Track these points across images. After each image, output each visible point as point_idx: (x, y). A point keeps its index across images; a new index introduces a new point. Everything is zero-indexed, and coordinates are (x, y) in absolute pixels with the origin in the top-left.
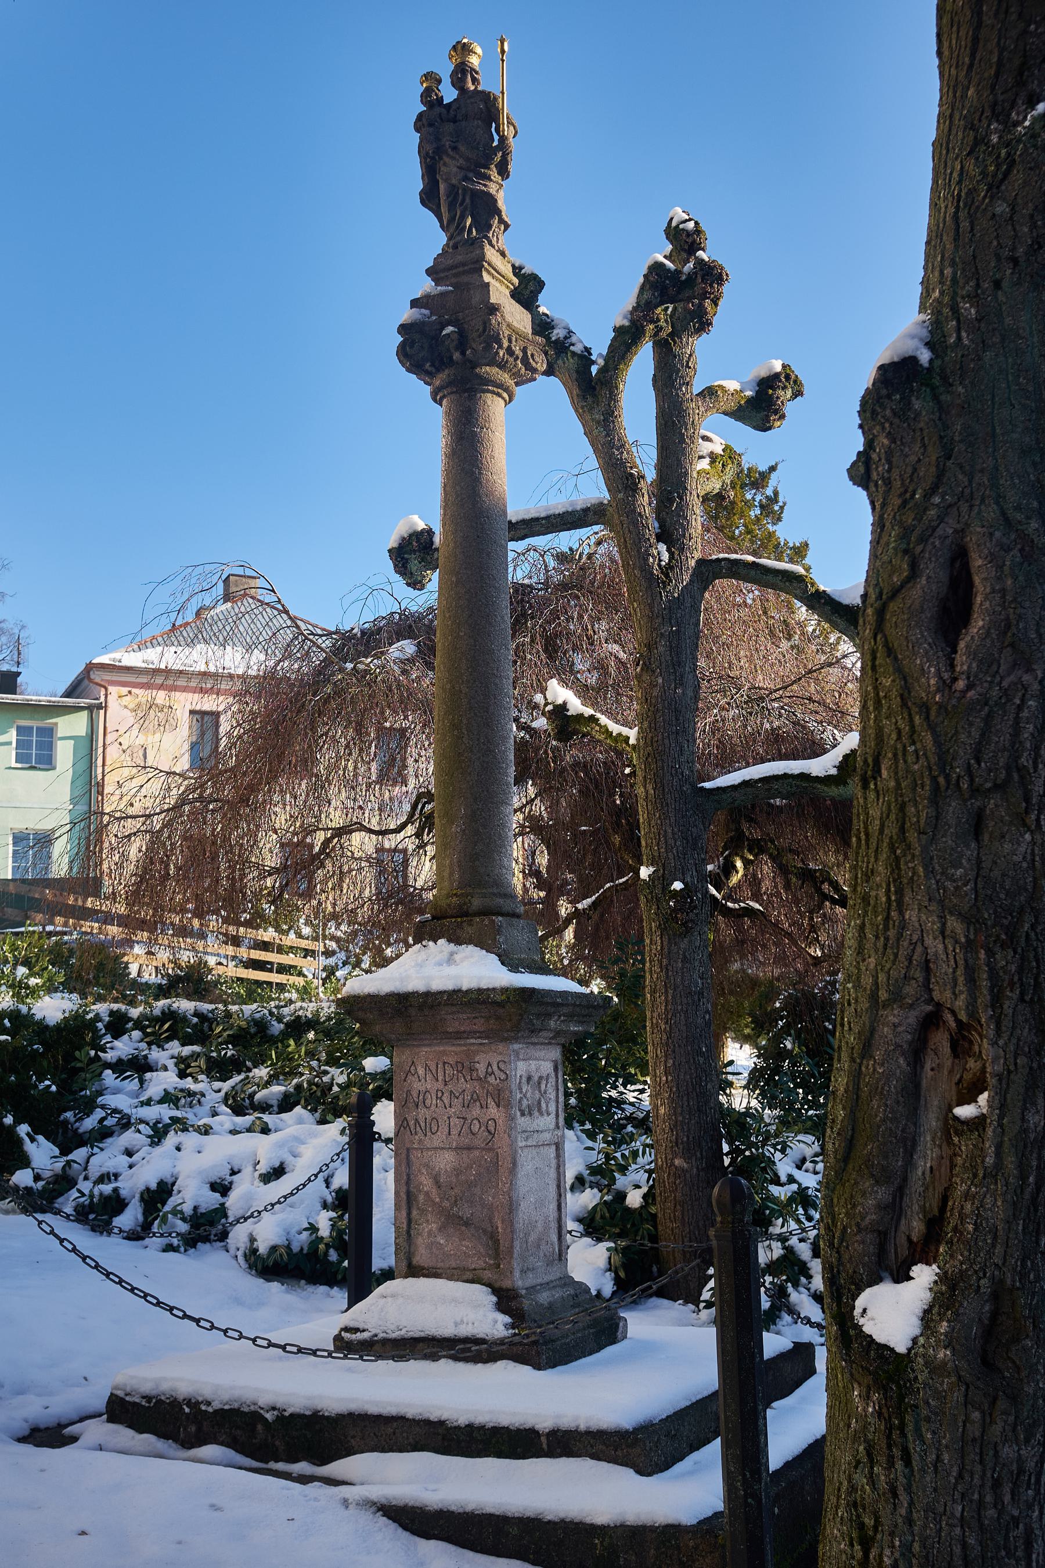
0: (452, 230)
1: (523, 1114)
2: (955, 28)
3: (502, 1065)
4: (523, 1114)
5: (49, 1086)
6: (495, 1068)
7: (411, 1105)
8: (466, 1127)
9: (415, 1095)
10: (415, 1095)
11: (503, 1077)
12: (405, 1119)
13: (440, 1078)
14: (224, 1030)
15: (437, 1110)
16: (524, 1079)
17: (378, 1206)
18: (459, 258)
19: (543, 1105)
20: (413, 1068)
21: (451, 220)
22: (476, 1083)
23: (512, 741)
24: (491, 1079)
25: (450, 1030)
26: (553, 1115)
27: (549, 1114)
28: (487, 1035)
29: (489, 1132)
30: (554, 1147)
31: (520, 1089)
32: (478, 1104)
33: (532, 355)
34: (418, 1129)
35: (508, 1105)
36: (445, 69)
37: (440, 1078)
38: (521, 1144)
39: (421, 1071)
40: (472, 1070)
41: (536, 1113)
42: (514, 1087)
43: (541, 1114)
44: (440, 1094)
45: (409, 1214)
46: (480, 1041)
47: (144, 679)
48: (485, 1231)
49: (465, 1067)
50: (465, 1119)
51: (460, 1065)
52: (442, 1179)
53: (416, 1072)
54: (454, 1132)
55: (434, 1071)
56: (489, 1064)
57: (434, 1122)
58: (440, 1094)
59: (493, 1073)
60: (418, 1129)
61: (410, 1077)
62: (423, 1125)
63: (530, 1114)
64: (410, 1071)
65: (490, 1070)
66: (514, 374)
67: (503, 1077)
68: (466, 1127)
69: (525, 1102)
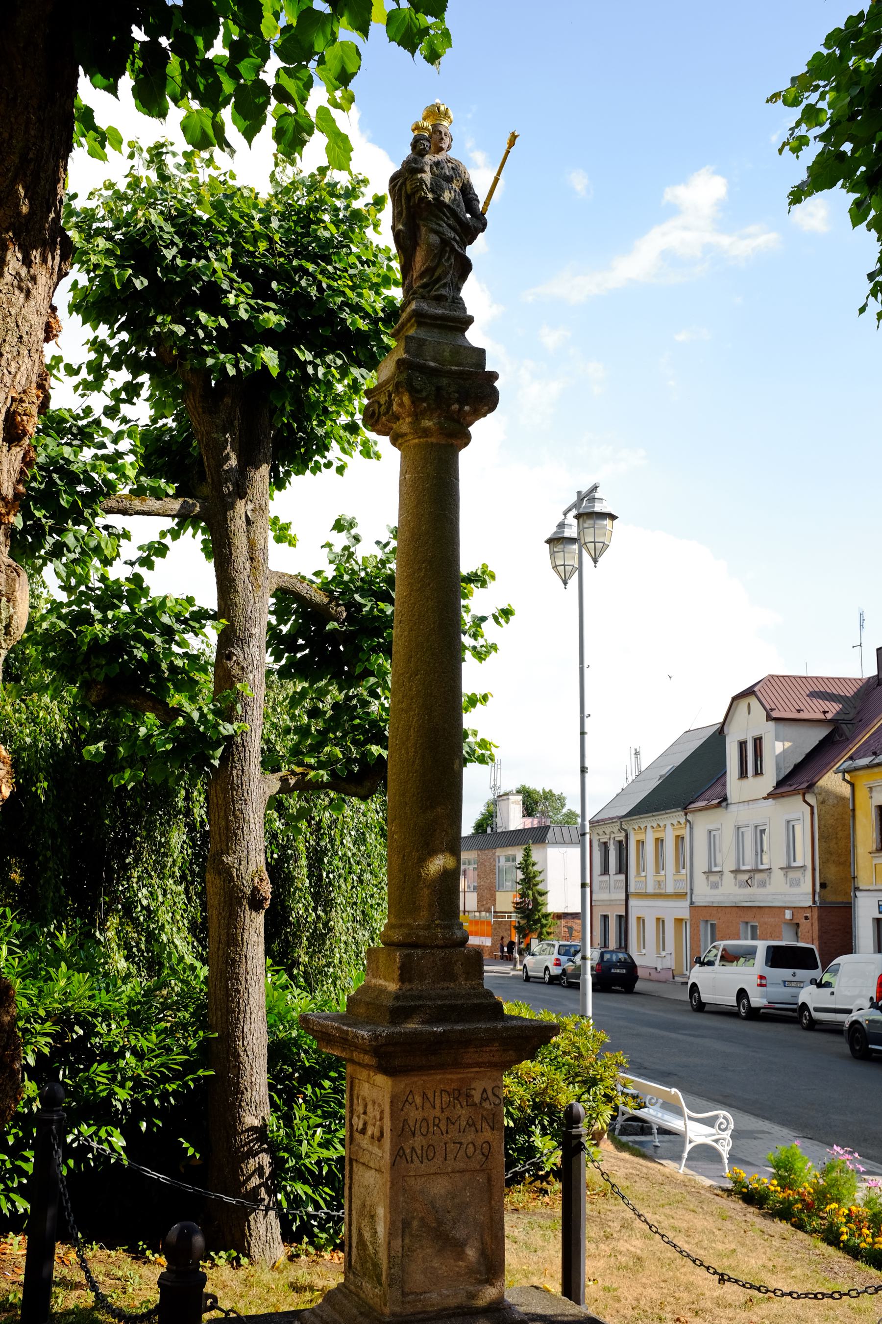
5: (69, 1103)
6: (489, 1092)
8: (461, 1153)
10: (411, 1123)
12: (402, 1147)
13: (438, 1105)
14: (305, 899)
15: (434, 1137)
20: (410, 1097)
23: (390, 784)
24: (486, 1105)
25: (153, 176)
29: (483, 1154)
32: (473, 1129)
34: (414, 1157)
37: (438, 1105)
39: (418, 1100)
40: (469, 1096)
44: (437, 1121)
47: (614, 903)
49: (461, 1094)
50: (461, 1144)
51: (456, 1092)
53: (414, 1101)
54: (450, 1156)
55: (431, 1100)
56: (485, 1090)
57: (424, 1124)
58: (437, 1121)
59: (487, 1098)
60: (414, 1157)
61: (407, 1106)
62: (419, 1152)
64: (407, 1100)
66: (271, 1032)
68: (461, 1153)
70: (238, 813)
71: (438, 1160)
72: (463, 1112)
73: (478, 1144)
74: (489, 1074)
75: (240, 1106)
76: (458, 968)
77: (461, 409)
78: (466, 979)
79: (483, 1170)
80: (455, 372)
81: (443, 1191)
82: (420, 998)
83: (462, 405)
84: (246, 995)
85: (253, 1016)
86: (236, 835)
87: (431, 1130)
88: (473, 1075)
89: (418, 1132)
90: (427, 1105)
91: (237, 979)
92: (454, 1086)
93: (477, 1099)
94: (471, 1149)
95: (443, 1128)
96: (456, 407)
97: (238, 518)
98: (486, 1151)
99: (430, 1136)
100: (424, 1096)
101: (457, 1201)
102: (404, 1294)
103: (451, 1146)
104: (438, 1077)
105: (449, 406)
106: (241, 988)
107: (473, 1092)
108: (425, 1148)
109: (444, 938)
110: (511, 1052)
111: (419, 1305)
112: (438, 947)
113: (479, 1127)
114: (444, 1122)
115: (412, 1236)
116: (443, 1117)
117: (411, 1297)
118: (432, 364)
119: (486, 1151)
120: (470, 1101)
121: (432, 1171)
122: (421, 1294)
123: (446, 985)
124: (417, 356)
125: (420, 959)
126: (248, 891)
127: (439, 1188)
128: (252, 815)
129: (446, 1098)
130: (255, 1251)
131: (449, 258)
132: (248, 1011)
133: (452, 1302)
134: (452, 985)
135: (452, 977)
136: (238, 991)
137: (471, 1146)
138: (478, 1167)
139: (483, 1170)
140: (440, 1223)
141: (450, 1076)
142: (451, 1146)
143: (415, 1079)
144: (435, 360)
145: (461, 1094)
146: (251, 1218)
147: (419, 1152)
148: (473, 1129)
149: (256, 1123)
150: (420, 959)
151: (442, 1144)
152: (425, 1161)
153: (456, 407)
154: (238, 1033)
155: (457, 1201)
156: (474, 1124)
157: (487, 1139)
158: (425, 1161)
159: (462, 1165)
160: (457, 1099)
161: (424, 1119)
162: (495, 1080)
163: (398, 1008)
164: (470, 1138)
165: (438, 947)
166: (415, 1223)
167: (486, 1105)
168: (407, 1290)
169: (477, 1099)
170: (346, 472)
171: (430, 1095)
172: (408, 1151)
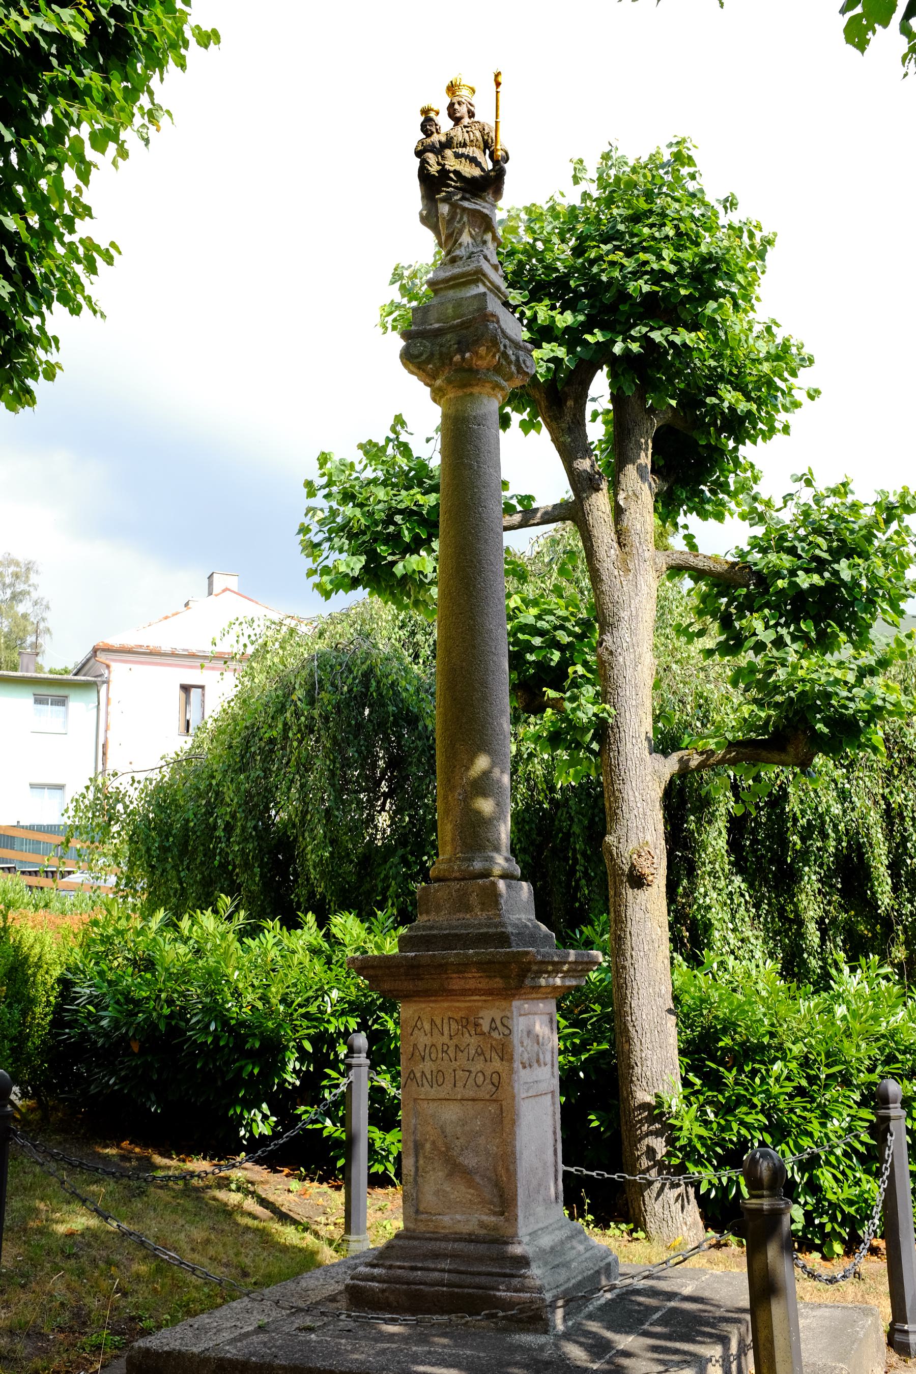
0: (450, 245)
1: (524, 1067)
2: (101, 742)
3: (505, 1021)
4: (524, 1067)
7: (417, 1057)
8: (471, 1081)
9: (421, 1049)
10: (421, 1049)
11: (507, 1032)
13: (446, 1032)
16: (525, 1034)
17: (695, 1224)
18: (457, 271)
19: (541, 1056)
21: (449, 236)
22: (480, 1038)
24: (495, 1034)
26: (549, 1066)
27: (545, 1065)
28: (490, 992)
30: (550, 1096)
31: (522, 1043)
32: (482, 1058)
33: (524, 361)
35: (511, 1060)
36: (441, 103)
37: (446, 1032)
38: (523, 1096)
39: (427, 1026)
40: (477, 1025)
41: (535, 1065)
42: (516, 1042)
43: (540, 1065)
44: (445, 1048)
45: (417, 1161)
46: (483, 998)
48: (489, 1179)
49: (469, 1023)
50: (470, 1072)
52: (448, 1130)
54: (460, 1084)
56: (493, 1020)
58: (445, 1048)
61: (416, 1031)
62: (429, 1077)
63: (530, 1066)
65: (419, 1023)
67: (507, 1032)
68: (471, 1081)
69: (526, 1056)
70: (617, 793)
71: (448, 1086)
72: (471, 1041)
73: (488, 1074)
74: (497, 1003)
75: (632, 1081)
76: (474, 899)
77: (463, 358)
78: (482, 910)
79: (495, 1101)
80: (457, 325)
81: (454, 1118)
82: (431, 928)
83: (463, 353)
84: (632, 970)
85: (641, 991)
86: (616, 814)
87: (440, 1055)
88: (480, 1004)
89: (427, 1058)
90: (435, 1031)
91: (623, 955)
92: (462, 1014)
93: (486, 1028)
94: (480, 1079)
95: (452, 1055)
96: (457, 358)
97: (595, 510)
98: (496, 1081)
99: (439, 1061)
100: (432, 1021)
101: (467, 1128)
102: (417, 1212)
103: (459, 1073)
104: (446, 1005)
105: (451, 359)
106: (628, 964)
107: (481, 1021)
108: (434, 1074)
109: (460, 870)
110: (497, 979)
111: (431, 1225)
112: (456, 879)
113: (488, 1057)
114: (452, 1049)
115: (425, 1157)
116: (451, 1043)
117: (423, 1217)
118: (437, 326)
119: (496, 1081)
120: (479, 1030)
121: (441, 1096)
122: (435, 1215)
123: (461, 915)
124: (422, 324)
125: (437, 891)
126: (626, 868)
127: (450, 1114)
128: (631, 793)
129: (454, 1026)
130: (651, 1226)
131: (461, 218)
132: (635, 987)
133: (465, 1229)
134: (468, 916)
135: (468, 909)
136: (624, 967)
137: (480, 1075)
138: (487, 1097)
139: (495, 1101)
140: (448, 1148)
141: (457, 1004)
142: (459, 1073)
143: (423, 1005)
144: (438, 321)
145: (469, 1023)
146: (645, 1194)
147: (429, 1077)
148: (482, 1058)
149: (650, 1099)
150: (437, 891)
151: (451, 1071)
152: (435, 1086)
153: (457, 358)
154: (627, 1009)
155: (467, 1128)
156: (483, 1053)
157: (497, 1069)
158: (435, 1086)
159: (470, 1094)
160: (465, 1027)
161: (433, 1045)
162: (504, 1010)
163: (411, 937)
164: (479, 1067)
165: (456, 879)
166: (428, 1146)
167: (495, 1034)
168: (421, 1209)
169: (486, 1028)
170: (792, 430)
171: (438, 1022)
172: (418, 1075)
